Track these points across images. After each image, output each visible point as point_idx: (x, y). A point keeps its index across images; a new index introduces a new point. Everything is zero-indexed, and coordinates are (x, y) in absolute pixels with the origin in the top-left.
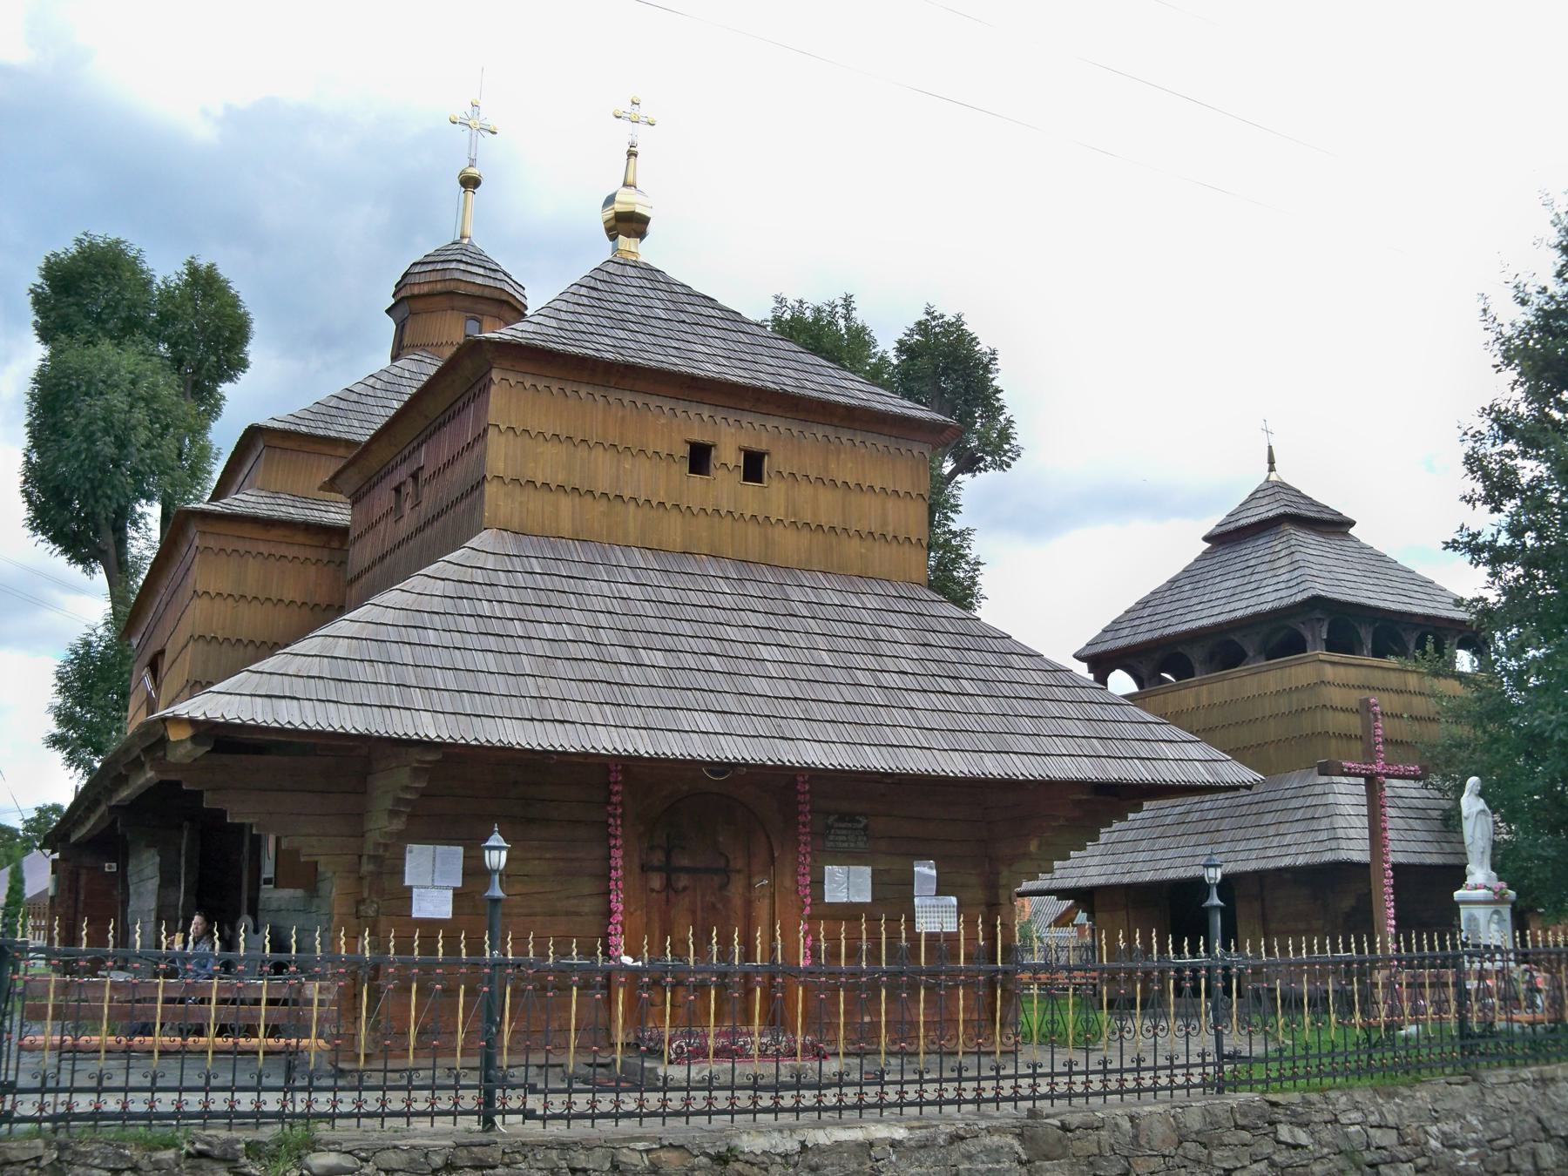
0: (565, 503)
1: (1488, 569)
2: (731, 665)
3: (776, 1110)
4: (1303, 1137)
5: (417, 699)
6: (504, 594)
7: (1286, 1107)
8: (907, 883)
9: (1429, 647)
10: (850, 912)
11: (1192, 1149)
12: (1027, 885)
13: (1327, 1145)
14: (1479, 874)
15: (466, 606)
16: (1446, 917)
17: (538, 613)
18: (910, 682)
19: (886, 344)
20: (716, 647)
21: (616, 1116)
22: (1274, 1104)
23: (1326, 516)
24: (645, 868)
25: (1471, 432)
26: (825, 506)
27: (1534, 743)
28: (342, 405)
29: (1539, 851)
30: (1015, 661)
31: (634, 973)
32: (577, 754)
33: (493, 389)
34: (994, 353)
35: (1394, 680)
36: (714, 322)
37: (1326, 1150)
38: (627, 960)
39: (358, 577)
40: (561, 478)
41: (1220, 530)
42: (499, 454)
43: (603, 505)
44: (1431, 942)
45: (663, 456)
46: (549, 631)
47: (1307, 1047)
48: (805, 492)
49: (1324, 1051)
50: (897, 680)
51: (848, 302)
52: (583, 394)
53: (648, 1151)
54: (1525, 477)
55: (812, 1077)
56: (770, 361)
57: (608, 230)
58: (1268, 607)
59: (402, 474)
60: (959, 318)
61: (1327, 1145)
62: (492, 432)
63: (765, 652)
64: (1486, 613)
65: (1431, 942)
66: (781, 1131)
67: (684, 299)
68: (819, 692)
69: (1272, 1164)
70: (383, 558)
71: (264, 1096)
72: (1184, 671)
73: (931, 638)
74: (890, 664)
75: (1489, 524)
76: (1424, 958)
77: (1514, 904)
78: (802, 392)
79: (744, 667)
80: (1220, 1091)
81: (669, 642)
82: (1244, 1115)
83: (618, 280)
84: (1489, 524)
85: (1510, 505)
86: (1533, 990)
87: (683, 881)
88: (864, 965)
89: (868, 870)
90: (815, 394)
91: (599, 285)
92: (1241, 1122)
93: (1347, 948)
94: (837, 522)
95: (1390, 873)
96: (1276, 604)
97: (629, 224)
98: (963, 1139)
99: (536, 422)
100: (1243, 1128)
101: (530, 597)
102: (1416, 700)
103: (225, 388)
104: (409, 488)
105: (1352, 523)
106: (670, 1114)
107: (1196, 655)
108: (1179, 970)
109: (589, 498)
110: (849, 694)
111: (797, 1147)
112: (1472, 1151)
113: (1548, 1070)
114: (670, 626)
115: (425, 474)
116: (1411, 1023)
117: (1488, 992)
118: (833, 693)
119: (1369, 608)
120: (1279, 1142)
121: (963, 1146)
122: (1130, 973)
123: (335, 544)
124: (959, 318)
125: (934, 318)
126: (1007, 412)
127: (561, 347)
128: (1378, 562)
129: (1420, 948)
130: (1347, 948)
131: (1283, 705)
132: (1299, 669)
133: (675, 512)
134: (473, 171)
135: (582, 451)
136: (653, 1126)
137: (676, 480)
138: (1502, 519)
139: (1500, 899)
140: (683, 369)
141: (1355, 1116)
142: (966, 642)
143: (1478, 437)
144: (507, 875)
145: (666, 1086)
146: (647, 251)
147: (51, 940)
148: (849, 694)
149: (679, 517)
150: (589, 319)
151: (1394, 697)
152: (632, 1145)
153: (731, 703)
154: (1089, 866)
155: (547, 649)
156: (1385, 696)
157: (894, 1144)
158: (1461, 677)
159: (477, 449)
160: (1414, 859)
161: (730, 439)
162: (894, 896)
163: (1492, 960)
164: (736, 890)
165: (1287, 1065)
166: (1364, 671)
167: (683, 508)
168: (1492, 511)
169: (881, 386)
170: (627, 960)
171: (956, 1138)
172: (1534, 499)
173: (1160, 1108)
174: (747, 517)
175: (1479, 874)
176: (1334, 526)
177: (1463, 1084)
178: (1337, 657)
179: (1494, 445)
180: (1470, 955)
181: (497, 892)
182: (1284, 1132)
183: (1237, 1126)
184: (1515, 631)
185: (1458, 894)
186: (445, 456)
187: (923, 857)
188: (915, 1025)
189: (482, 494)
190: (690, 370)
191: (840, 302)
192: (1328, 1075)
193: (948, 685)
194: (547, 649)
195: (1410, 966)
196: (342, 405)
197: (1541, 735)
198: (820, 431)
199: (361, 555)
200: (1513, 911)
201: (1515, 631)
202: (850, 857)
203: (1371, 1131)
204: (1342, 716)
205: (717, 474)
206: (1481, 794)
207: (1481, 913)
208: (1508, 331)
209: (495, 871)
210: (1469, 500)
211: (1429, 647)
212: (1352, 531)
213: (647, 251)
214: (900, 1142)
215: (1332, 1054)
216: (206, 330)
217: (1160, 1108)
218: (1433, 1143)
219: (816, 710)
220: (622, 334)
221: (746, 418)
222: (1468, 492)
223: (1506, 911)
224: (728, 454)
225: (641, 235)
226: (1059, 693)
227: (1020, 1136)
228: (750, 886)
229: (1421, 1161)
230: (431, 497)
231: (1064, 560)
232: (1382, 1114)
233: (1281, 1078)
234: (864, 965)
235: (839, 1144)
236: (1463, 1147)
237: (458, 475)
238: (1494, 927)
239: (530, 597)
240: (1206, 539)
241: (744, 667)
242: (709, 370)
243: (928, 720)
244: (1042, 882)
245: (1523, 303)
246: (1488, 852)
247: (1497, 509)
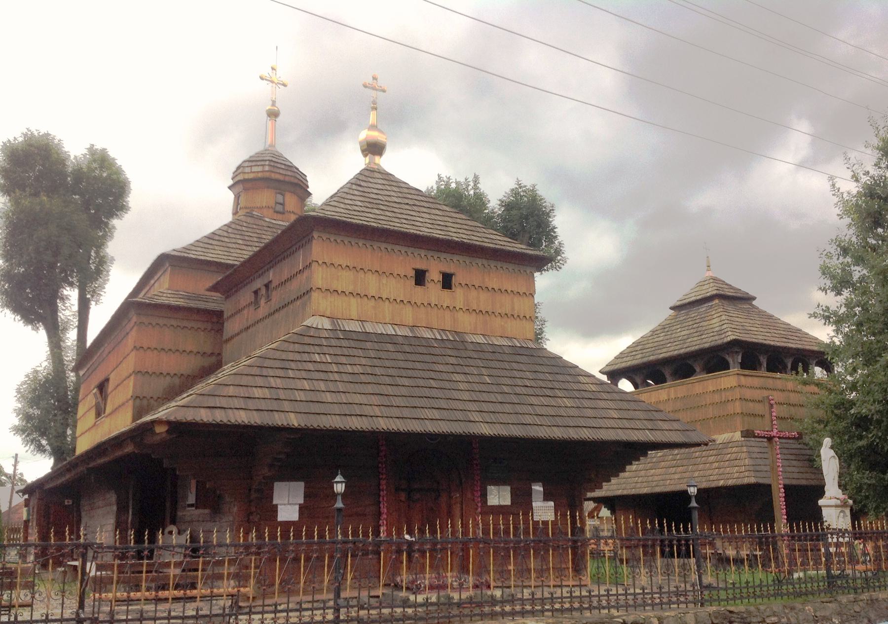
0: (353, 301)
1: (834, 327)
5: (286, 406)
6: (325, 350)
7: (738, 613)
8: (529, 494)
9: (800, 369)
10: (499, 510)
12: (590, 495)
15: (306, 357)
16: (816, 515)
17: (343, 360)
18: (530, 391)
22: (731, 612)
23: (739, 295)
24: (397, 489)
25: (825, 253)
26: (482, 300)
27: (863, 422)
28: (211, 242)
29: (866, 481)
30: (581, 379)
31: (410, 544)
32: (369, 431)
33: (314, 241)
39: (232, 338)
40: (350, 288)
42: (319, 277)
43: (372, 303)
46: (349, 369)
50: (524, 390)
51: (476, 179)
54: (856, 276)
59: (258, 284)
60: (534, 186)
62: (314, 265)
63: (457, 377)
64: (836, 351)
67: (406, 191)
68: (485, 397)
70: (248, 328)
72: (660, 379)
75: (834, 302)
76: (806, 536)
77: (851, 507)
78: (471, 242)
79: (447, 385)
85: (846, 293)
86: (865, 554)
87: (417, 496)
89: (509, 488)
90: (478, 243)
93: (766, 530)
94: (489, 309)
95: (783, 490)
102: (792, 395)
103: (115, 222)
104: (263, 291)
105: (754, 298)
107: (667, 372)
108: (679, 541)
109: (365, 298)
113: (875, 595)
117: (842, 554)
118: (492, 397)
119: (765, 345)
122: (654, 541)
123: (215, 320)
125: (520, 188)
126: (560, 239)
127: (349, 220)
128: (769, 320)
129: (805, 530)
130: (766, 530)
131: (717, 398)
133: (409, 304)
137: (404, 289)
138: (841, 299)
139: (844, 504)
140: (412, 231)
142: (556, 370)
143: (829, 256)
144: (344, 496)
149: (411, 308)
150: (359, 203)
151: (779, 393)
154: (614, 487)
156: (775, 393)
158: (818, 384)
160: (794, 482)
162: (522, 500)
164: (443, 499)
166: (762, 379)
167: (413, 303)
168: (836, 296)
169: (495, 230)
170: (407, 537)
172: (860, 287)
173: (673, 614)
175: (833, 493)
177: (830, 602)
178: (747, 372)
179: (838, 259)
180: (832, 534)
184: (851, 361)
185: (821, 502)
186: (286, 276)
187: (536, 481)
188: (529, 570)
189: (310, 297)
190: (415, 232)
191: (471, 178)
193: (548, 392)
196: (211, 242)
197: (866, 416)
199: (231, 327)
200: (851, 510)
201: (851, 361)
202: (499, 482)
204: (751, 404)
206: (832, 447)
209: (338, 494)
210: (824, 290)
212: (754, 303)
215: (760, 586)
216: (99, 192)
217: (673, 614)
220: (377, 212)
222: (823, 286)
223: (848, 512)
224: (434, 275)
226: (605, 396)
228: (451, 497)
230: (277, 297)
233: (734, 598)
237: (294, 287)
240: (671, 308)
242: (425, 231)
243: (539, 410)
244: (598, 493)
245: (857, 180)
247: (839, 293)
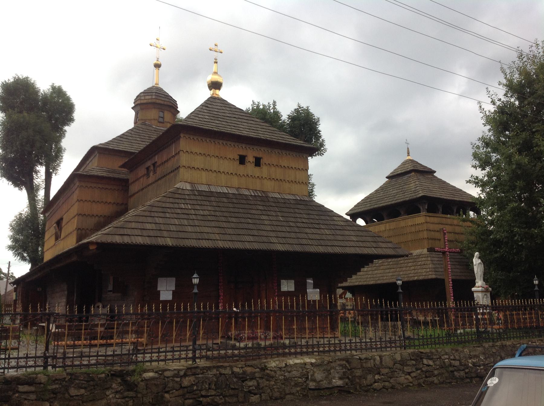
0: (204, 174)
1: (481, 189)
2: (254, 221)
4: (431, 363)
5: (165, 234)
6: (188, 201)
7: (425, 353)
10: (288, 293)
11: (398, 366)
12: (340, 285)
13: (438, 365)
14: (480, 283)
15: (176, 206)
18: (305, 225)
19: (284, 117)
20: (249, 216)
25: (475, 146)
26: (278, 173)
27: (497, 243)
30: (335, 218)
33: (181, 139)
34: (318, 119)
35: (449, 221)
36: (244, 117)
38: (235, 309)
40: (202, 166)
41: (391, 175)
42: (184, 159)
44: (467, 304)
46: (201, 212)
47: (371, 339)
48: (273, 169)
49: (436, 336)
50: (302, 225)
52: (208, 141)
56: (261, 130)
58: (407, 199)
59: (149, 163)
60: (308, 107)
62: (181, 153)
65: (467, 304)
68: (280, 229)
69: (422, 371)
70: (143, 189)
73: (311, 212)
74: (299, 220)
75: (480, 174)
79: (258, 222)
80: (405, 349)
81: (236, 215)
82: (413, 356)
83: (214, 104)
84: (480, 174)
88: (196, 309)
89: (293, 281)
91: (209, 106)
92: (412, 358)
94: (282, 178)
95: (451, 282)
96: (411, 198)
98: (331, 362)
99: (195, 150)
100: (413, 360)
101: (195, 202)
102: (457, 227)
103: (66, 128)
104: (152, 168)
105: (435, 172)
106: (188, 358)
108: (391, 311)
109: (211, 172)
110: (288, 229)
111: (284, 365)
112: (482, 367)
114: (236, 210)
115: (158, 164)
116: (469, 328)
117: (485, 319)
120: (424, 364)
124: (308, 107)
126: (323, 137)
131: (413, 229)
132: (418, 218)
135: (208, 158)
139: (487, 291)
140: (237, 133)
141: (446, 357)
142: (320, 213)
144: (198, 285)
148: (288, 229)
150: (207, 117)
153: (255, 233)
154: (354, 280)
155: (202, 218)
156: (446, 226)
157: (312, 364)
159: (176, 158)
161: (251, 155)
163: (486, 309)
165: (425, 340)
166: (439, 219)
171: (329, 362)
173: (388, 353)
175: (480, 283)
176: (429, 173)
177: (479, 347)
178: (431, 214)
179: (483, 149)
181: (196, 291)
182: (425, 361)
186: (165, 159)
189: (179, 171)
191: (271, 103)
192: (437, 344)
194: (202, 218)
195: (461, 311)
198: (276, 151)
199: (134, 188)
200: (491, 294)
202: (287, 278)
203: (452, 361)
204: (433, 233)
205: (248, 164)
206: (479, 258)
207: (480, 295)
208: (487, 113)
210: (475, 167)
211: (461, 213)
212: (435, 174)
213: (223, 94)
215: (438, 337)
216: (57, 110)
217: (388, 353)
218: (470, 365)
219: (280, 234)
220: (217, 122)
221: (255, 147)
223: (489, 294)
224: (250, 159)
225: (219, 89)
226: (349, 228)
227: (347, 361)
229: (467, 370)
230: (160, 171)
231: (340, 184)
232: (454, 356)
233: (423, 345)
234: (196, 309)
235: (296, 364)
236: (479, 366)
237: (170, 165)
238: (485, 299)
239: (195, 202)
240: (387, 178)
241: (258, 222)
242: (245, 133)
245: (494, 104)
246: (482, 276)
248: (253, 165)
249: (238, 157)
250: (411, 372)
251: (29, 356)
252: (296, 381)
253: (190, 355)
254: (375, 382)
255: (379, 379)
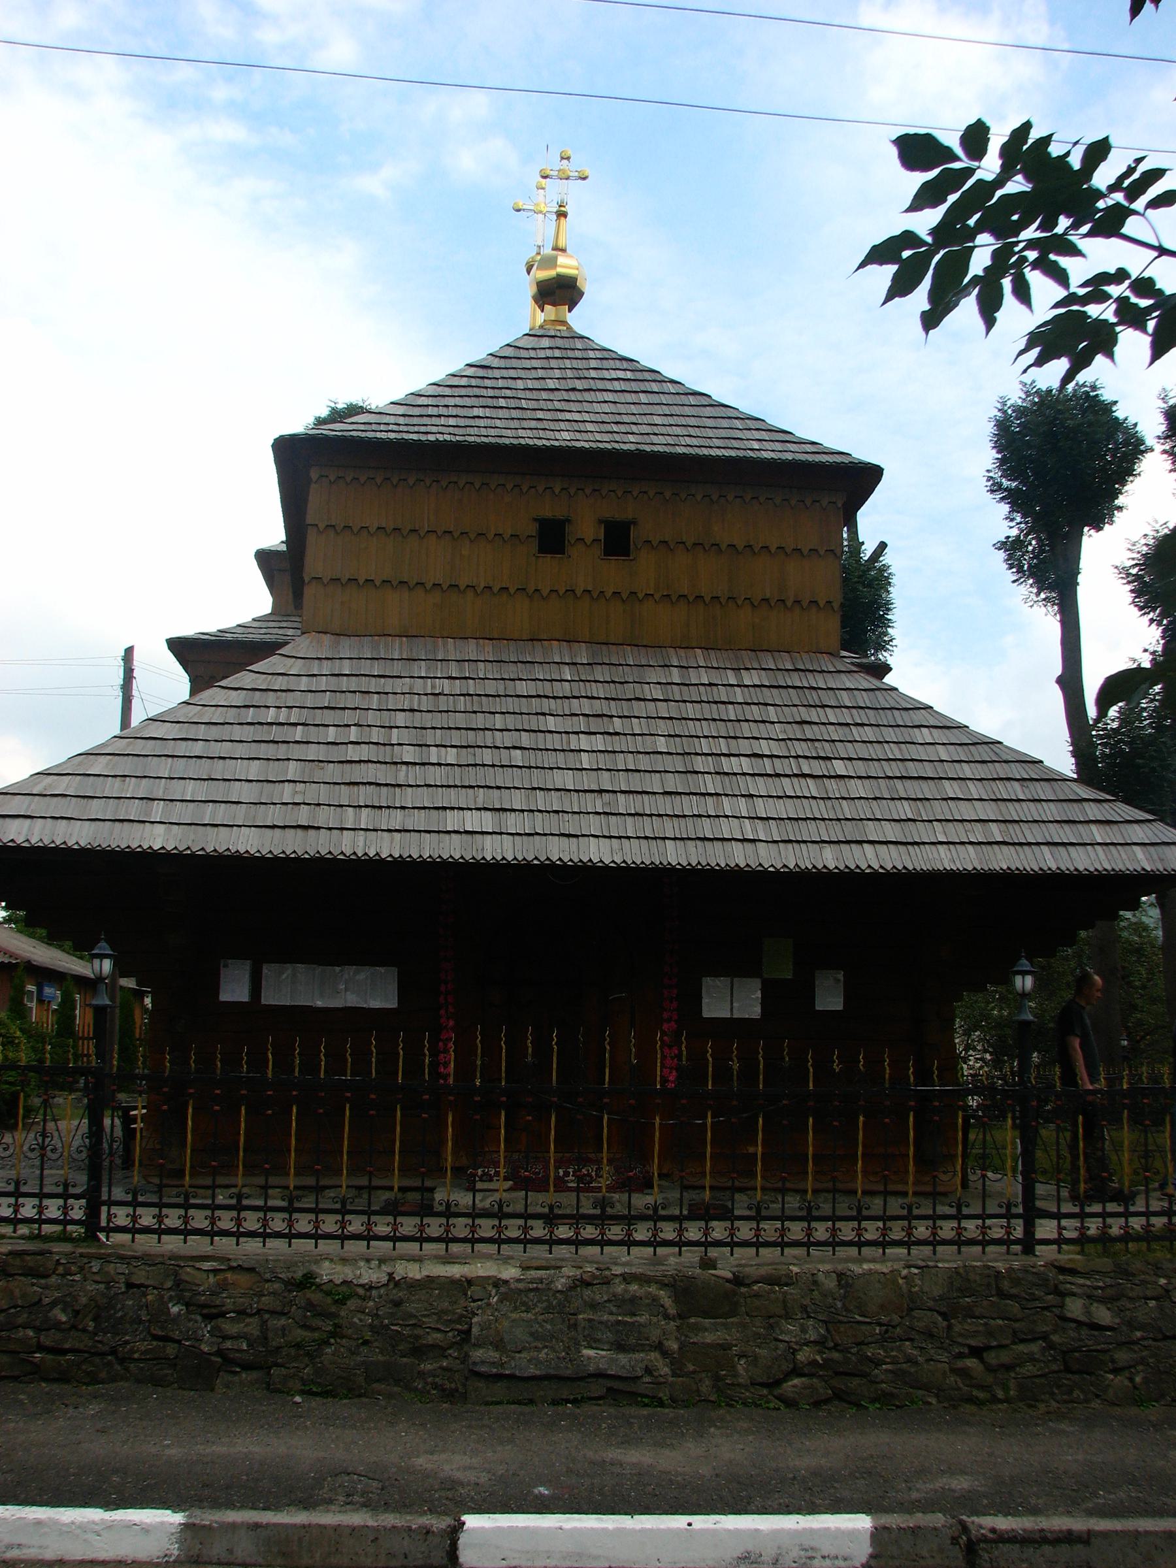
3: (369, 1237)
21: (186, 1232)
37: (1138, 1334)
45: (507, 537)
53: (215, 1271)
55: (620, 1209)
57: (536, 301)
61: (1141, 1327)
66: (368, 1261)
69: (1051, 1346)
71: (964, 1223)
97: (559, 292)
98: (588, 1284)
111: (385, 1279)
121: (587, 1292)
134: (566, 265)
136: (225, 1245)
145: (449, 1212)
146: (579, 319)
147: (75, 1046)
152: (198, 1265)
174: (608, 594)
183: (1002, 1294)
193: (817, 768)
213: (579, 319)
214: (506, 1282)
224: (586, 528)
225: (572, 305)
248: (598, 550)
249: (532, 529)
250: (988, 1348)
251: (506, 1209)
252: (417, 1337)
253: (1019, 1233)
254: (796, 1372)
255: (814, 1363)
